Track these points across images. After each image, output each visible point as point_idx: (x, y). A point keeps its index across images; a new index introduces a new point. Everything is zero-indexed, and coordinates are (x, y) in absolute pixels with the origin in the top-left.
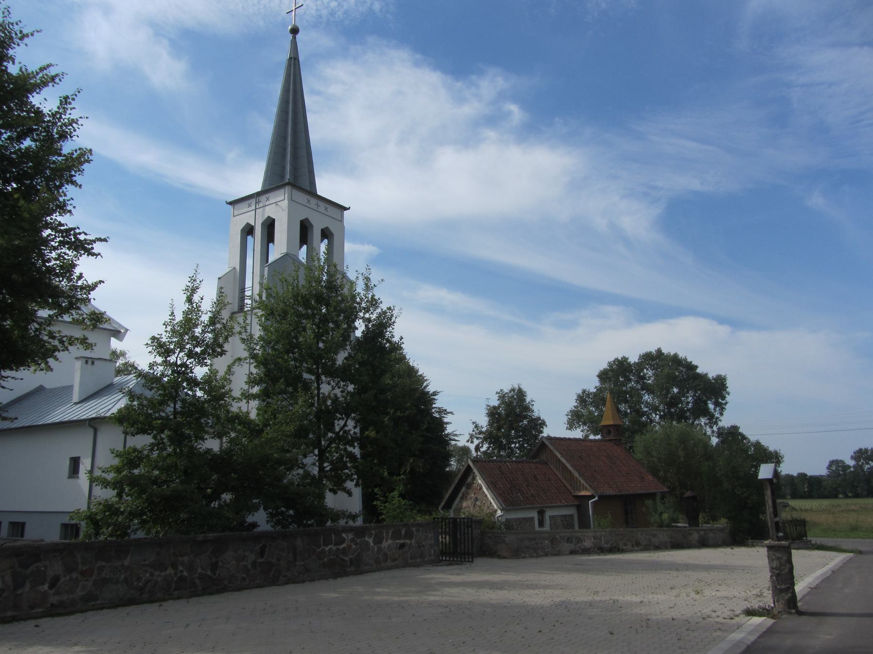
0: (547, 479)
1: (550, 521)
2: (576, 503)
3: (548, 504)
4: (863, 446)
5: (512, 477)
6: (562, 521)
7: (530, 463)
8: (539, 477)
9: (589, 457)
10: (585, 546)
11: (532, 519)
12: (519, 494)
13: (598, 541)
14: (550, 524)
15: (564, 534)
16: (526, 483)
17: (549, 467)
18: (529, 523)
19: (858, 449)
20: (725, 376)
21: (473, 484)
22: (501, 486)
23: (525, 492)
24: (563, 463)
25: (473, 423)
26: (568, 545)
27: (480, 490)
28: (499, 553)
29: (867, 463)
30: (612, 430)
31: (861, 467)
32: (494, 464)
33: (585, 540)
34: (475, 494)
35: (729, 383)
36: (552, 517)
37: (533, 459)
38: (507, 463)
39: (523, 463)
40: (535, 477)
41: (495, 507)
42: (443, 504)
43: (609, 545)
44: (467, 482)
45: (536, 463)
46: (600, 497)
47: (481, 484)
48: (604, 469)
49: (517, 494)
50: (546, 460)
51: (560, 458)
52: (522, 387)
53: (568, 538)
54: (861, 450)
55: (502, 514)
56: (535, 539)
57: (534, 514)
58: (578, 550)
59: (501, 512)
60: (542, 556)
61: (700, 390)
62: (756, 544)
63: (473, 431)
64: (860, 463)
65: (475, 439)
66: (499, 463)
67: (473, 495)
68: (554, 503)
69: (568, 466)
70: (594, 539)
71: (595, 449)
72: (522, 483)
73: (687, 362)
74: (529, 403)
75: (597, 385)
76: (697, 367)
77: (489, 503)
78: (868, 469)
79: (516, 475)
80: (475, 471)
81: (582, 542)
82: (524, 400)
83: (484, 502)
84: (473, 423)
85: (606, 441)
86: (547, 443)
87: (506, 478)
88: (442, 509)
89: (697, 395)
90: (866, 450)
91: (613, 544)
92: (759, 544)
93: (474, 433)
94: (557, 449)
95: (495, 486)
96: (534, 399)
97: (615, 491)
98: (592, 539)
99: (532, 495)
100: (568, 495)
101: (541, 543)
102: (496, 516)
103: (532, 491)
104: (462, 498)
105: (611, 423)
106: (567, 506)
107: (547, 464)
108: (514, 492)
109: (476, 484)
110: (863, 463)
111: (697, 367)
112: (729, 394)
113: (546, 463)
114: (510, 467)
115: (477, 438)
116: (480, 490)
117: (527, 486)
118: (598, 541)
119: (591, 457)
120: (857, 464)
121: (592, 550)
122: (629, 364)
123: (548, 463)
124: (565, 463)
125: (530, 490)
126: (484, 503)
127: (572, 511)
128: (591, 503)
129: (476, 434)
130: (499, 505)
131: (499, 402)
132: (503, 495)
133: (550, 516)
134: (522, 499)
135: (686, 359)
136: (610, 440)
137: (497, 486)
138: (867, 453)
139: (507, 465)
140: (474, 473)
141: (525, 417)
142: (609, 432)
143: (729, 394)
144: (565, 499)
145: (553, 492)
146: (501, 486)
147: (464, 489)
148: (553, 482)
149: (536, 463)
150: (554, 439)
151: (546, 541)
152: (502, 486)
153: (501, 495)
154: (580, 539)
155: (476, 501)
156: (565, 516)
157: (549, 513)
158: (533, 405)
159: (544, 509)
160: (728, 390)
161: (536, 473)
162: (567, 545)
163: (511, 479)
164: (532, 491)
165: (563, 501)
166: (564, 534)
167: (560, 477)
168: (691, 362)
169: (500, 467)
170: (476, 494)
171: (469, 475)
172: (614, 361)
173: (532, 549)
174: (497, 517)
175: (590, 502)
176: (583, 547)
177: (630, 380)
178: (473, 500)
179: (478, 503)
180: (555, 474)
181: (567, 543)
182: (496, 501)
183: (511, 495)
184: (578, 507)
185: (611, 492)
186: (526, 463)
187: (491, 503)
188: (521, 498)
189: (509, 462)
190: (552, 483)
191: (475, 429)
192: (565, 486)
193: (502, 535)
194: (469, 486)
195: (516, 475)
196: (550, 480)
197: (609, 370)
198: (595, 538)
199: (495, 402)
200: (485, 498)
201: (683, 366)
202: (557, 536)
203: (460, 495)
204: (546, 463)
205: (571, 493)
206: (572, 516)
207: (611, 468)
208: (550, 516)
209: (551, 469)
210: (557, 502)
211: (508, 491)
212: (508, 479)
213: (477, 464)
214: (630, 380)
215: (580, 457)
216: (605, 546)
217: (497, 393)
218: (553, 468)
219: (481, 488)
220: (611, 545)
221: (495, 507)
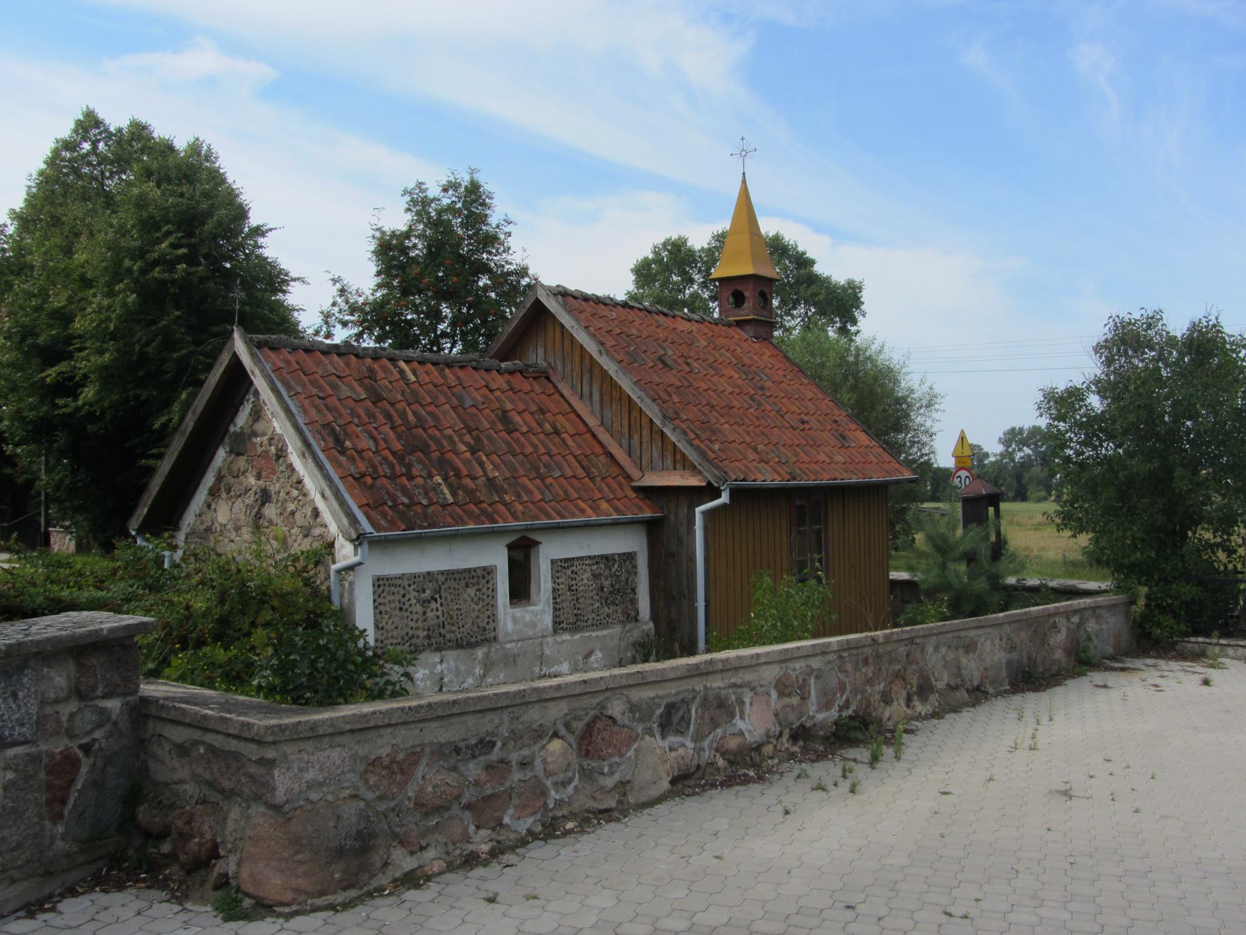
0: (547, 426)
1: (554, 578)
2: (648, 514)
3: (563, 517)
4: (1017, 425)
5: (415, 413)
6: (596, 576)
7: (488, 370)
8: (517, 419)
9: (688, 364)
10: (741, 733)
11: (488, 573)
12: (439, 479)
13: (795, 700)
14: (554, 590)
15: (648, 693)
16: (468, 438)
17: (555, 387)
18: (471, 591)
19: (1009, 428)
20: (860, 282)
21: (255, 434)
22: (366, 443)
23: (465, 472)
24: (604, 374)
25: (335, 281)
26: (666, 744)
27: (278, 457)
28: (232, 869)
29: (1020, 450)
30: (747, 294)
31: (1010, 455)
32: (347, 364)
33: (741, 703)
34: (259, 477)
35: (865, 296)
36: (560, 566)
37: (502, 360)
38: (402, 364)
39: (462, 367)
40: (504, 417)
41: (333, 528)
42: (143, 511)
43: (833, 714)
44: (232, 429)
45: (511, 373)
46: (734, 493)
47: (281, 439)
48: (736, 404)
49: (431, 476)
50: (545, 364)
51: (595, 355)
52: (481, 178)
53: (670, 708)
54: (1013, 429)
55: (357, 559)
56: (486, 744)
57: (496, 557)
58: (712, 764)
59: (356, 554)
60: (532, 835)
61: (815, 304)
62: (1217, 649)
63: (334, 304)
64: (1010, 450)
65: (339, 326)
66: (369, 361)
67: (252, 481)
68: (573, 515)
69: (626, 384)
70: (781, 694)
71: (704, 343)
72: (456, 439)
73: (797, 252)
74: (498, 227)
75: (630, 290)
76: (812, 262)
77: (309, 511)
78: (1022, 458)
79: (432, 408)
80: (259, 382)
81: (732, 716)
82: (483, 219)
83: (291, 507)
84: (335, 281)
85: (729, 325)
86: (552, 305)
87: (389, 417)
88: (141, 531)
89: (810, 314)
90: (1021, 430)
91: (846, 705)
92: (1231, 652)
93: (336, 309)
94: (586, 328)
95: (338, 441)
96: (512, 218)
97: (779, 474)
98: (774, 694)
99: (491, 482)
100: (620, 485)
101: (524, 764)
102: (334, 567)
103: (489, 467)
104: (214, 492)
105: (748, 270)
106: (615, 524)
107: (548, 378)
108: (415, 472)
109: (264, 434)
110: (1014, 450)
111: (812, 262)
112: (864, 315)
113: (543, 375)
114: (413, 378)
115: (345, 324)
116: (278, 457)
117: (473, 451)
118: (795, 700)
119: (695, 364)
120: (1007, 450)
121: (768, 749)
122: (691, 252)
123: (553, 378)
124: (612, 373)
125: (481, 465)
126: (293, 513)
127: (632, 543)
128: (704, 513)
129: (340, 311)
130: (345, 521)
131: (409, 216)
132: (369, 480)
133: (553, 562)
134: (450, 499)
135: (797, 247)
136: (739, 324)
137: (348, 443)
138: (1022, 434)
139: (402, 372)
140: (257, 393)
141: (484, 269)
142: (739, 299)
143: (864, 315)
144: (608, 501)
145: (569, 473)
146: (366, 443)
147: (221, 454)
148: (570, 442)
149: (511, 373)
150: (575, 298)
151: (556, 745)
152: (371, 444)
153: (359, 479)
154: (722, 704)
155: (263, 504)
156: (607, 559)
157: (550, 551)
158: (509, 234)
159: (536, 537)
160: (863, 307)
161: (509, 406)
162: (657, 743)
163: (411, 417)
164: (489, 467)
165: (604, 505)
166: (648, 693)
167: (592, 422)
168: (804, 253)
169: (372, 375)
170: (264, 474)
171: (241, 403)
172: (665, 244)
173: (468, 807)
174: (339, 572)
175: (698, 510)
176: (733, 743)
177: (692, 281)
178: (250, 500)
179: (270, 511)
180: (574, 411)
181: (663, 737)
182: (335, 505)
183: (404, 480)
184: (653, 528)
185: (768, 478)
186: (475, 369)
187: (316, 513)
188: (446, 491)
189: (407, 362)
190: (563, 440)
191: (339, 300)
192: (611, 456)
193: (252, 751)
194: (240, 446)
195: (432, 408)
196: (557, 433)
197: (654, 261)
198: (783, 688)
199: (398, 220)
200: (295, 493)
201: (789, 257)
202: (616, 708)
203: (209, 479)
204: (543, 375)
205: (629, 478)
206: (630, 557)
207: (753, 400)
208: (553, 562)
209: (562, 396)
210: (582, 511)
211: (391, 466)
212: (399, 421)
213: (272, 354)
214: (692, 281)
215: (660, 359)
216: (820, 717)
217: (406, 192)
218: (566, 391)
219: (281, 454)
220: (841, 709)
221: (333, 528)
